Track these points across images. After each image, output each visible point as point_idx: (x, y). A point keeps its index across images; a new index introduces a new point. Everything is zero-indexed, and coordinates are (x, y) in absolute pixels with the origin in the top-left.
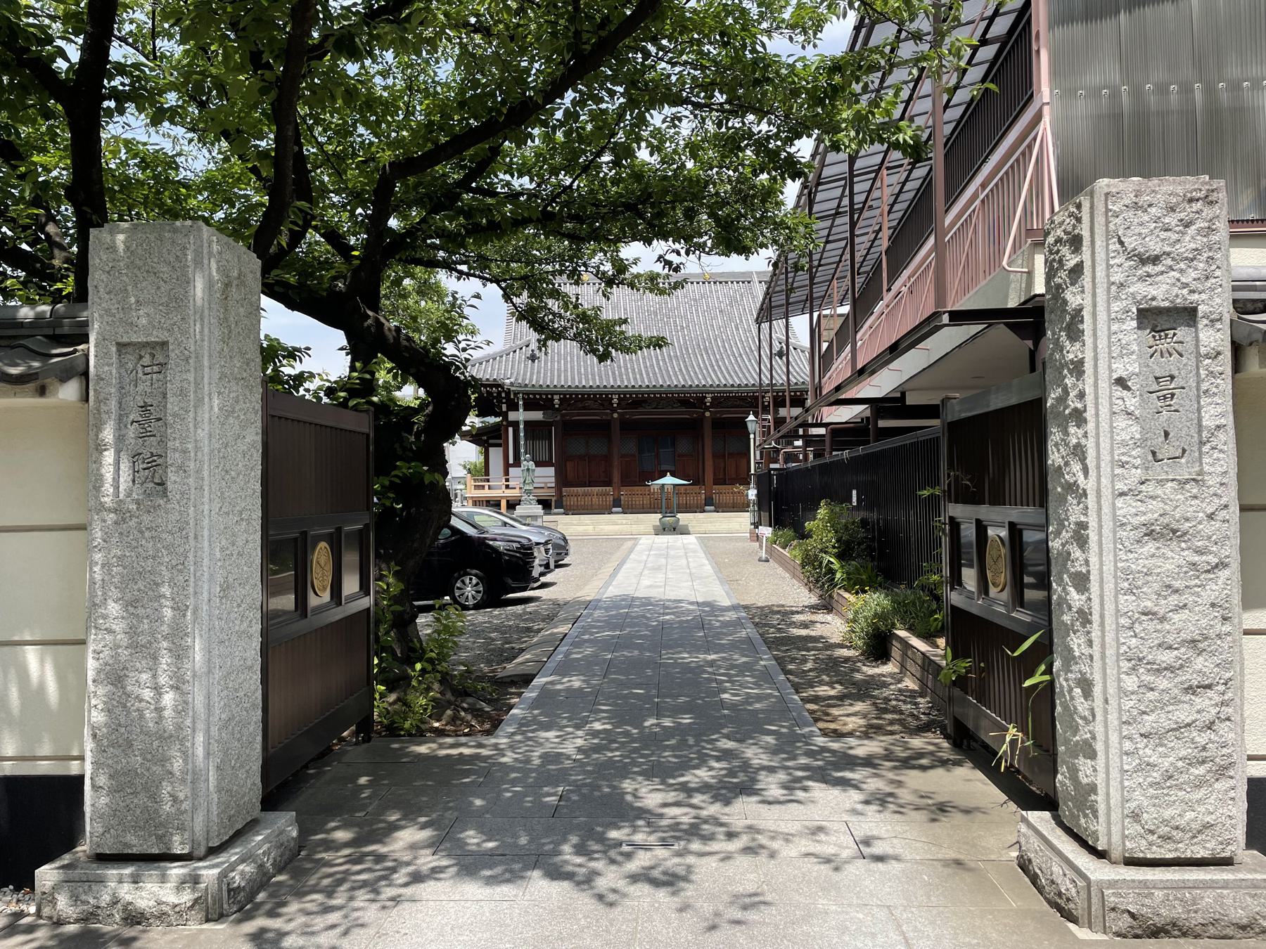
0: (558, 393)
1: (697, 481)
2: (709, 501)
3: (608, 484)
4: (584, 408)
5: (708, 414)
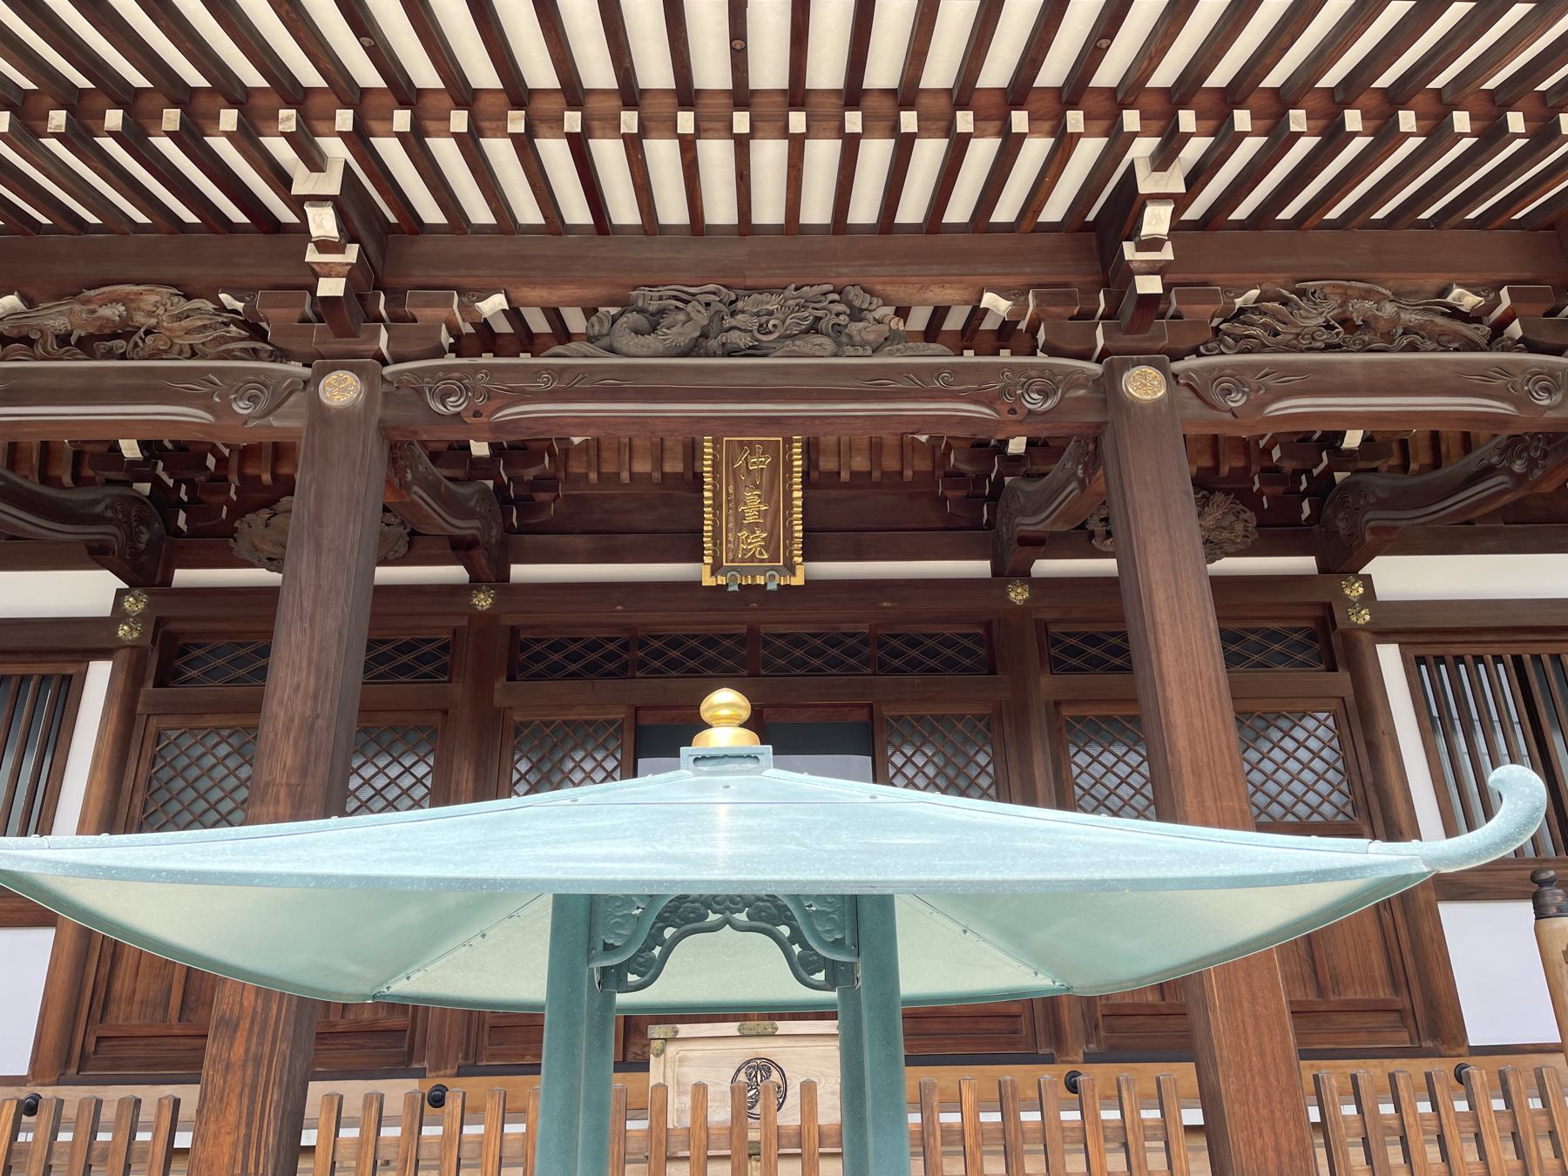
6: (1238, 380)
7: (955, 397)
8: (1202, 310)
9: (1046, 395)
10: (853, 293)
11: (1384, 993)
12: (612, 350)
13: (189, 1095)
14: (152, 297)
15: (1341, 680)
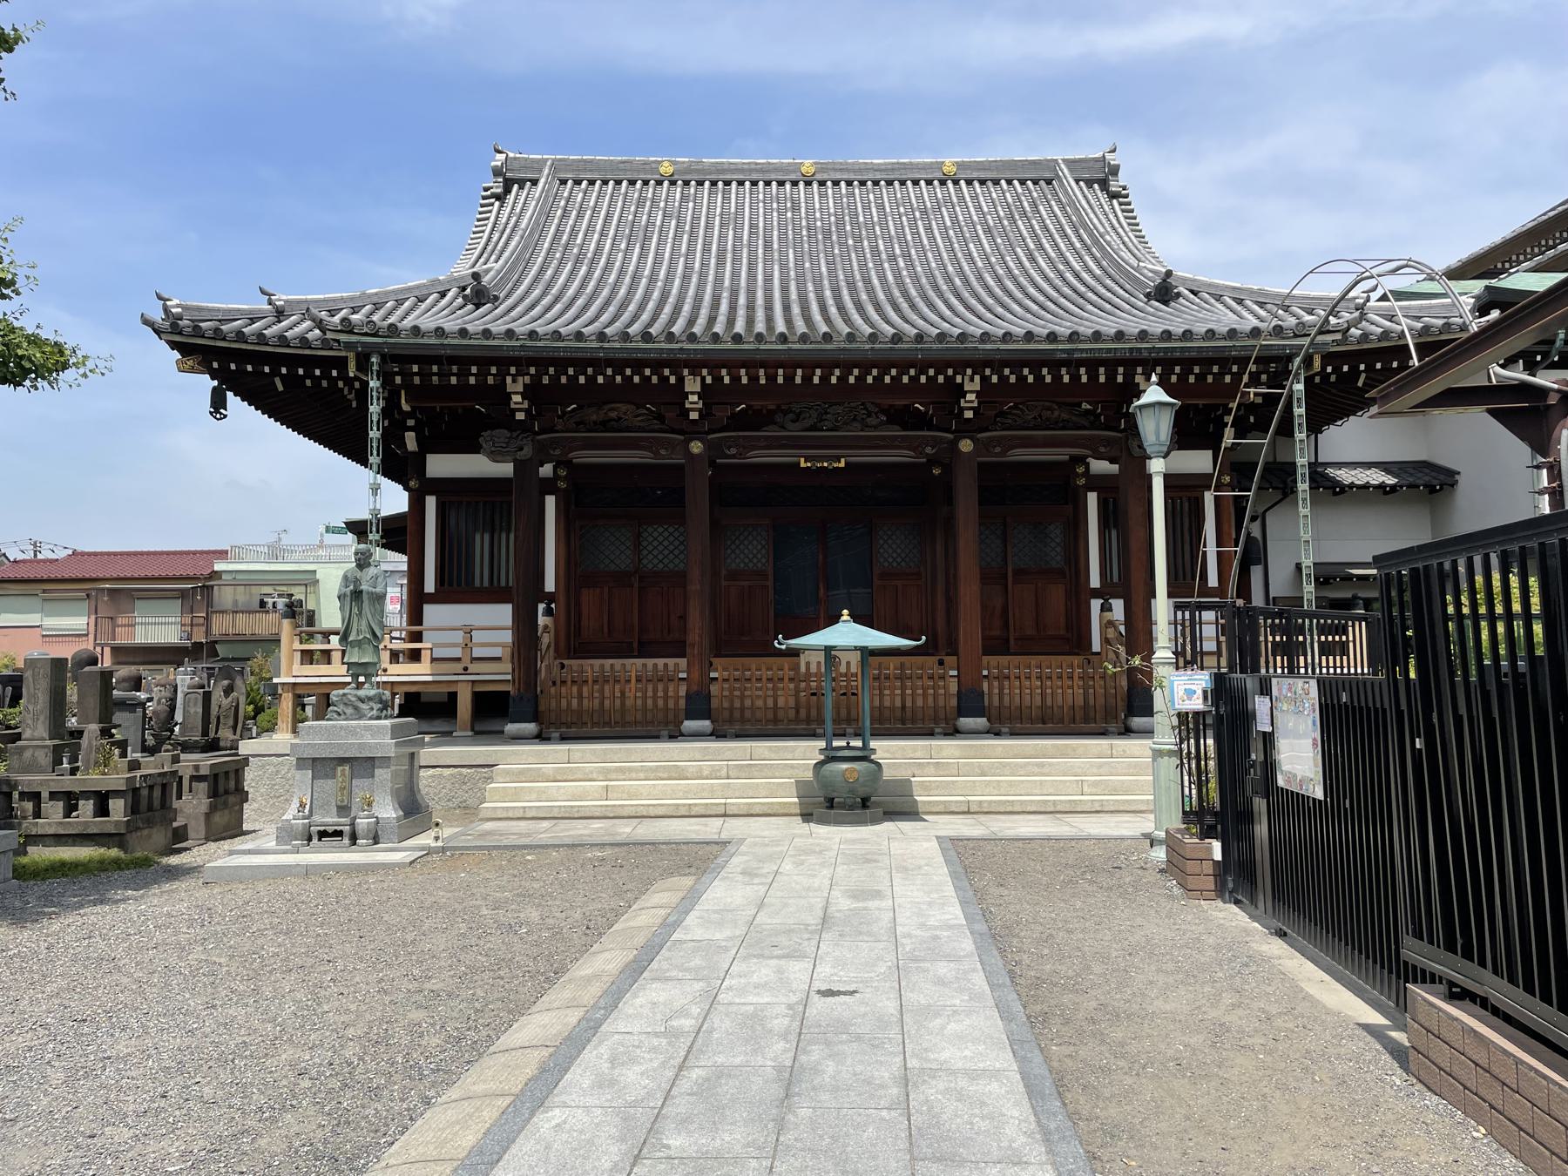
0: (979, 364)
1: (940, 644)
2: (971, 702)
3: (677, 649)
4: (605, 425)
5: (966, 446)
11: (1062, 632)
13: (683, 662)
14: (623, 407)
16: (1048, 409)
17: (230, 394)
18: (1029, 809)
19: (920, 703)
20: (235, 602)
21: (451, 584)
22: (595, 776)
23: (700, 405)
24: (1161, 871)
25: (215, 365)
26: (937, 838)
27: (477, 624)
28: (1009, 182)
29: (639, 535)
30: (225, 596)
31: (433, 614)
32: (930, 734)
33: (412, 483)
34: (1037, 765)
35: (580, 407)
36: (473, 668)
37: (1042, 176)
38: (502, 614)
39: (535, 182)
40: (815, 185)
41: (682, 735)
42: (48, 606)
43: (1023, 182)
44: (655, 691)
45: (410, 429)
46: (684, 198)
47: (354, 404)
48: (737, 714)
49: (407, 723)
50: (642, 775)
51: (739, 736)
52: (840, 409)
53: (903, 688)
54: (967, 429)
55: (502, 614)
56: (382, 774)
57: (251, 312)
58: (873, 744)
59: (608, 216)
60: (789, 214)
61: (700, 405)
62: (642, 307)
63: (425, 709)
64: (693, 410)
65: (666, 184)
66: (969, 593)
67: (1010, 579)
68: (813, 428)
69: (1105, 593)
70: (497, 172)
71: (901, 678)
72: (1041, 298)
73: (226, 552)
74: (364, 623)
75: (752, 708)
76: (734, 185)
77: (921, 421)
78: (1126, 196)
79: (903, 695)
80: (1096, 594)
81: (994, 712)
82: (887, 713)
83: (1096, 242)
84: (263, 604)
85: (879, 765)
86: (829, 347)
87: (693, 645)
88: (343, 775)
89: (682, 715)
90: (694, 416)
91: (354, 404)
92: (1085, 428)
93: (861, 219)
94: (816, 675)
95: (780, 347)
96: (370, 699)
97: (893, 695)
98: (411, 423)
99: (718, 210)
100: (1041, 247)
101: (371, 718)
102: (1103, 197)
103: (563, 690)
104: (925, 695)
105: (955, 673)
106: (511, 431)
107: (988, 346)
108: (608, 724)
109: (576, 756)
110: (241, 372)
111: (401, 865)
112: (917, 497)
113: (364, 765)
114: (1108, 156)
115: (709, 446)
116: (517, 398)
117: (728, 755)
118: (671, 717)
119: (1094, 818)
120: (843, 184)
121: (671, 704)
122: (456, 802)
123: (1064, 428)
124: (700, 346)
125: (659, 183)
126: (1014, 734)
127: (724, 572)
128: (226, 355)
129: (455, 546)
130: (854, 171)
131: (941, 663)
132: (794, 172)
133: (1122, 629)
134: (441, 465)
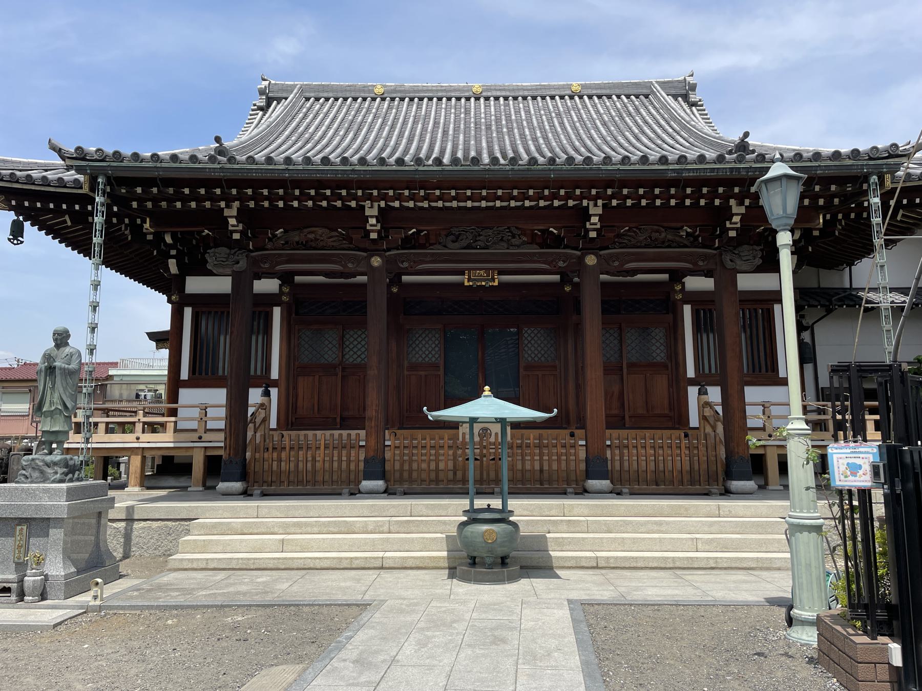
2: (596, 467)
4: (299, 245)
6: (616, 257)
7: (539, 262)
8: (611, 235)
9: (564, 262)
10: (513, 229)
11: (667, 412)
12: (445, 246)
13: (363, 433)
14: (320, 231)
15: (670, 317)
16: (657, 231)
17: (27, 224)
18: (651, 565)
19: (555, 467)
20: (121, 395)
21: (200, 374)
22: (276, 530)
23: (379, 227)
24: (811, 660)
25: (13, 203)
26: (570, 601)
27: (211, 402)
28: (618, 97)
29: (343, 336)
30: (114, 391)
31: (186, 395)
32: (563, 493)
33: (173, 297)
34: (656, 523)
35: (286, 231)
36: (206, 437)
37: (643, 92)
38: (218, 396)
39: (286, 99)
40: (482, 100)
41: (360, 492)
42: (5, 396)
43: (628, 97)
44: (340, 456)
45: (173, 257)
46: (390, 108)
47: (129, 238)
48: (406, 475)
49: (98, 485)
50: (316, 529)
51: (406, 494)
52: (490, 232)
53: (541, 455)
54: (592, 246)
55: (218, 396)
56: (57, 534)
57: (45, 165)
58: (514, 503)
59: (335, 118)
60: (462, 116)
61: (379, 227)
62: (327, 146)
63: (168, 470)
64: (373, 231)
65: (378, 100)
66: (594, 376)
67: (625, 370)
68: (468, 247)
69: (702, 381)
70: (262, 92)
71: (539, 446)
72: (652, 135)
73: (117, 363)
74: (56, 395)
75: (420, 470)
76: (426, 100)
77: (557, 242)
78: (702, 106)
79: (541, 460)
80: (692, 382)
81: (616, 475)
82: (528, 475)
83: (684, 128)
84: (138, 396)
85: (515, 525)
86: (476, 168)
87: (371, 419)
88: (21, 534)
89: (361, 474)
90: (374, 236)
91: (129, 238)
92: (685, 246)
93: (513, 117)
94: (494, 444)
95: (435, 168)
96: (55, 464)
97: (533, 460)
98: (173, 252)
99: (413, 114)
100: (643, 133)
101: (54, 482)
102: (685, 106)
103: (266, 455)
104: (559, 461)
105: (583, 443)
106: (230, 248)
107: (609, 167)
108: (300, 483)
109: (263, 512)
110: (33, 208)
111: (43, 628)
112: (554, 308)
113: (38, 525)
114: (688, 79)
115: (387, 261)
116: (232, 221)
117: (392, 511)
118: (352, 477)
119: (711, 576)
120: (501, 99)
121: (352, 467)
122: (162, 550)
123: (669, 247)
124: (370, 168)
125: (374, 99)
126: (634, 494)
127: (406, 364)
128: (21, 194)
129: (207, 347)
130: (509, 90)
131: (572, 435)
132: (468, 91)
133: (719, 409)
134: (195, 285)
